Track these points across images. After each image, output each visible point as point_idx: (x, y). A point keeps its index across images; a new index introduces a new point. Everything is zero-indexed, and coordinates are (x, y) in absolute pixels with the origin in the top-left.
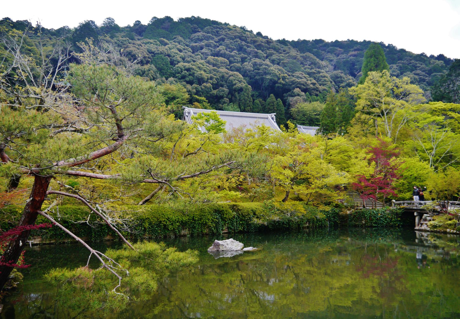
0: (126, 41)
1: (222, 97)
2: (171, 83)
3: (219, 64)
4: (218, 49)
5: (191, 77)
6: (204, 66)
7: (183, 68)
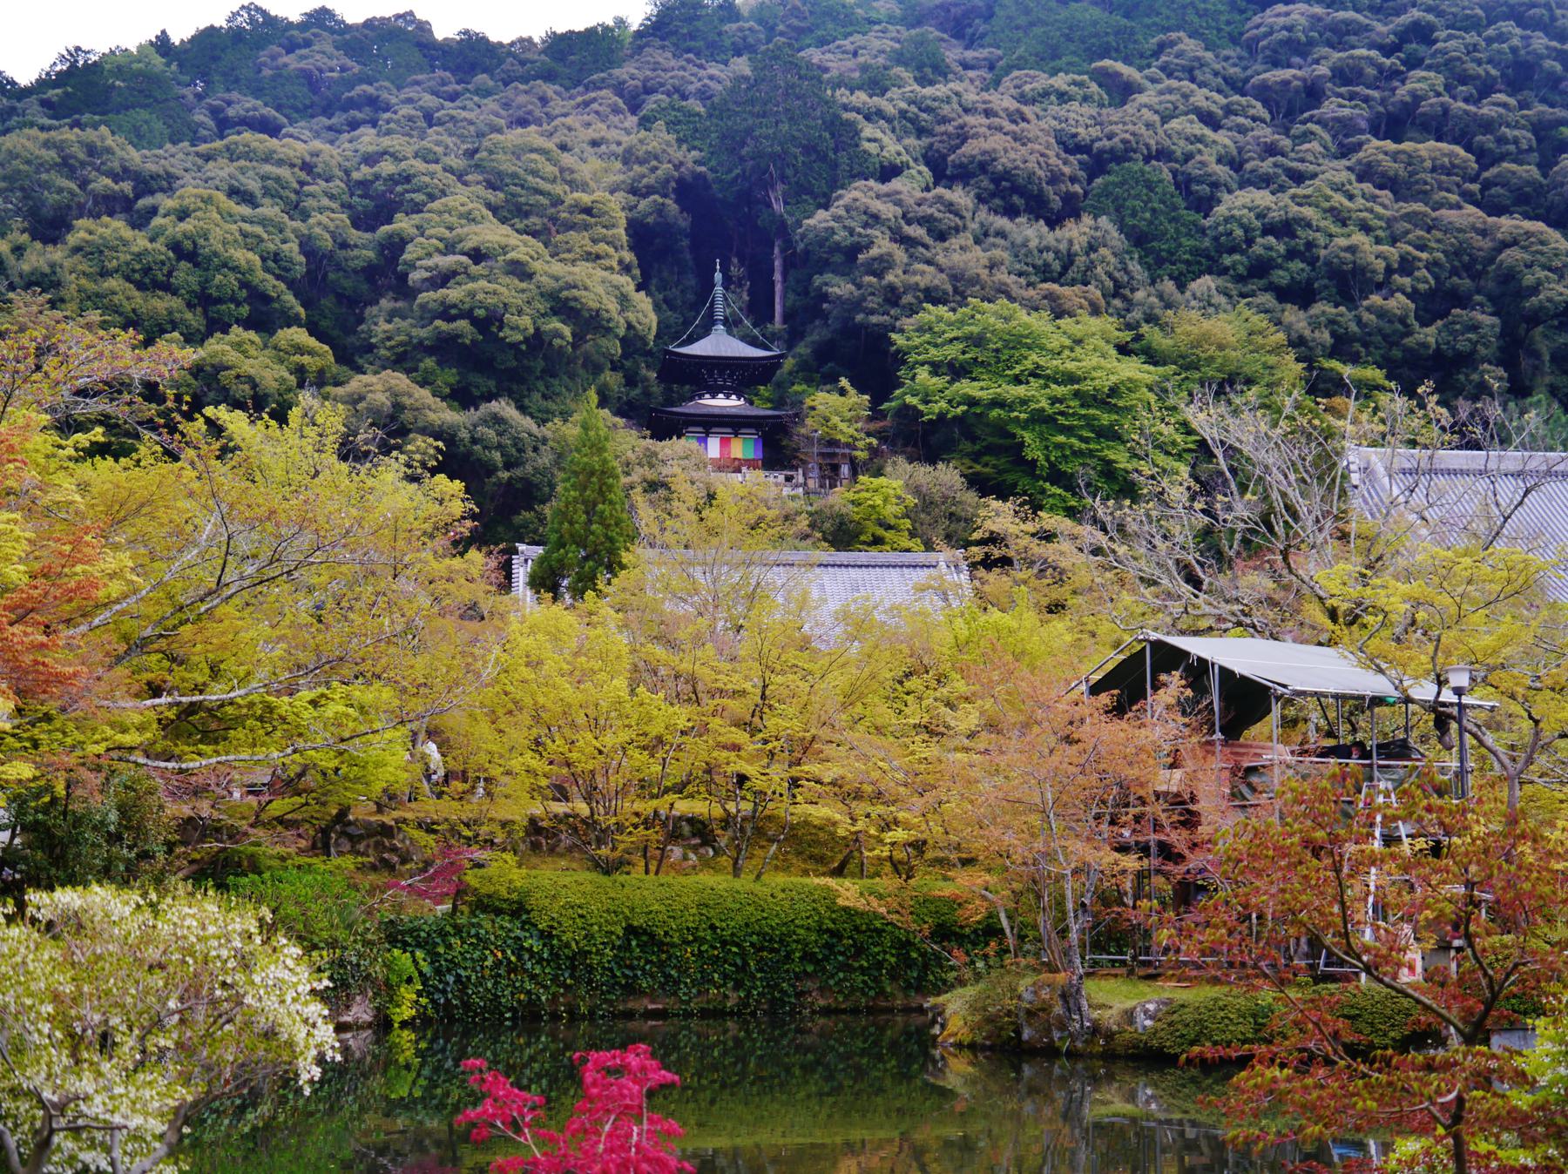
0: (948, 100)
1: (1467, 360)
2: (1207, 305)
3: (1428, 177)
4: (1402, 92)
5: (1297, 265)
6: (1351, 197)
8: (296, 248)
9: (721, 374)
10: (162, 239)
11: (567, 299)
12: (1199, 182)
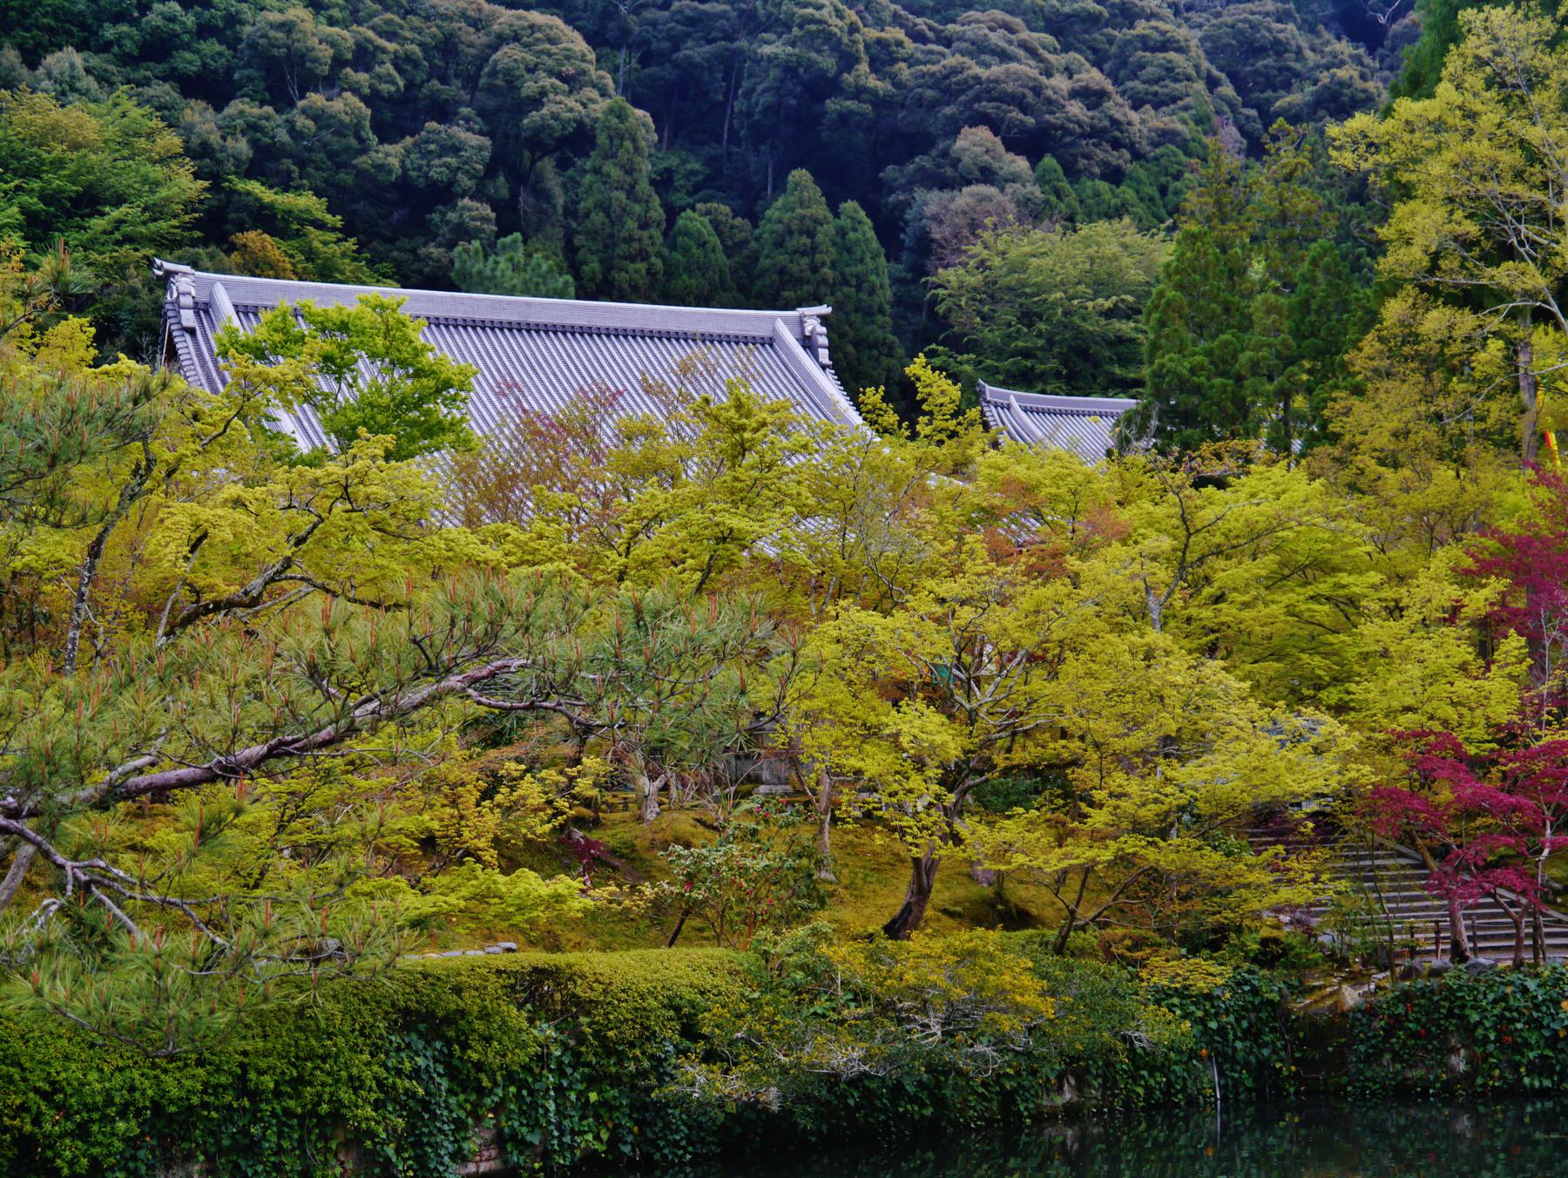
2: (66, 90)
5: (211, 47)
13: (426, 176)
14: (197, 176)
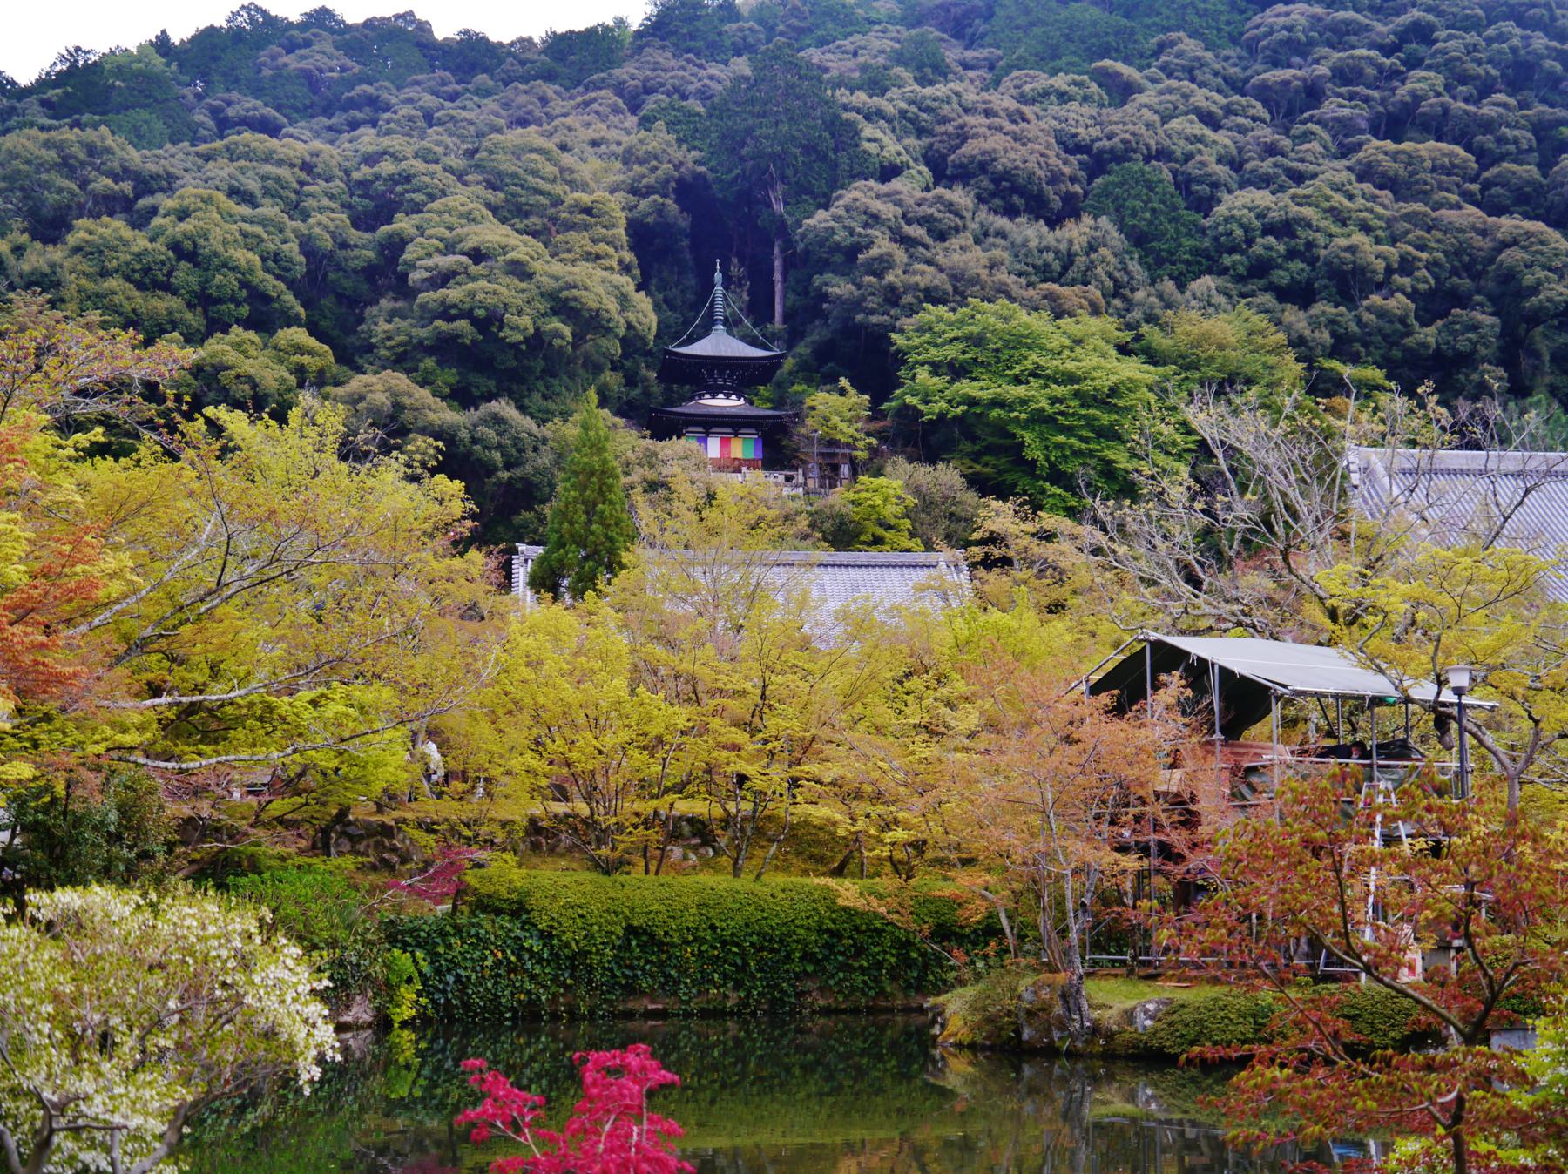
0: (948, 100)
1: (1467, 360)
2: (1207, 305)
4: (1402, 92)
5: (1297, 265)
6: (1351, 197)
7: (1258, 224)
8: (296, 248)
9: (721, 374)
10: (162, 239)
11: (567, 299)
12: (1199, 182)
13: (1454, 348)
14: (1298, 360)
